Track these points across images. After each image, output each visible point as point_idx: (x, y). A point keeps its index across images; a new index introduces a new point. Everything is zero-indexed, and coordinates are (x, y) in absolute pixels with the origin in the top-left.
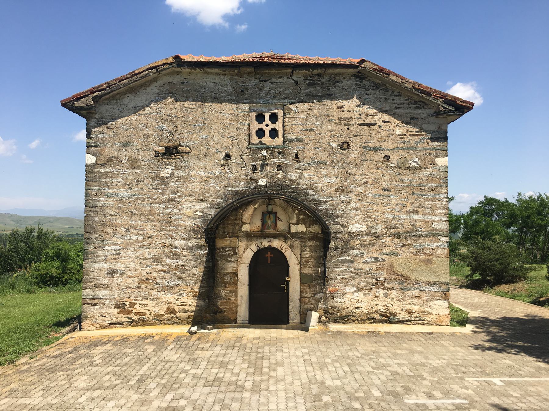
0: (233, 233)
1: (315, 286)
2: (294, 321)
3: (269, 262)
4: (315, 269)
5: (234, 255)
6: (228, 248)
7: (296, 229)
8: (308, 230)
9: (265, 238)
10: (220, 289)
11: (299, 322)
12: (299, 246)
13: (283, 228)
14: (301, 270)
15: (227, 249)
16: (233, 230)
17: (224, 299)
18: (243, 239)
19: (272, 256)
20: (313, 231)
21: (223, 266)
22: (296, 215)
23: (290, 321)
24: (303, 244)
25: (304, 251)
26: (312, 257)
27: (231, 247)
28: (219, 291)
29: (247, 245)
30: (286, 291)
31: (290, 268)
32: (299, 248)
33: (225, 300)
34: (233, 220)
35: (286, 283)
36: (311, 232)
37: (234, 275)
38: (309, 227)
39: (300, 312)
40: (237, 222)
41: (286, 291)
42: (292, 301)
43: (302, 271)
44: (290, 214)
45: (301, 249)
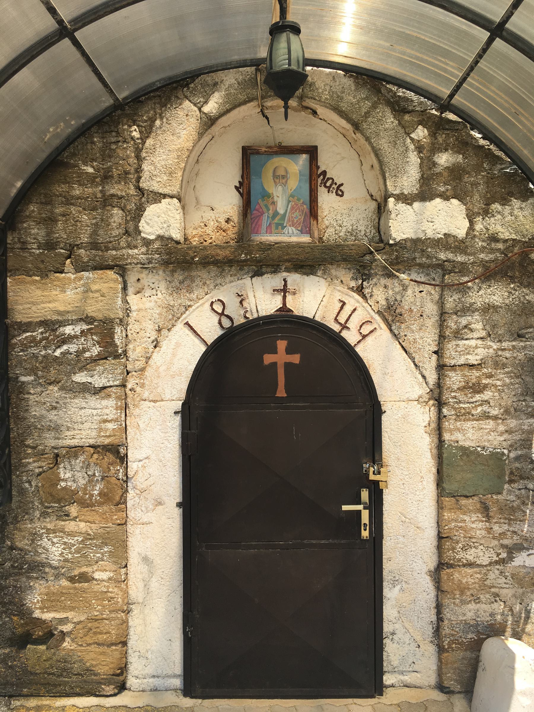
0: (94, 245)
1: (513, 510)
2: (407, 678)
3: (281, 392)
4: (513, 423)
5: (101, 358)
6: (73, 323)
7: (419, 222)
8: (479, 227)
9: (258, 273)
10: (38, 526)
11: (432, 679)
12: (431, 308)
13: (348, 224)
14: (439, 430)
15: (68, 330)
16: (95, 233)
17: (57, 577)
18: (147, 279)
19: (296, 359)
20: (505, 234)
21: (52, 416)
22: (419, 149)
23: (388, 679)
24: (451, 301)
25: (458, 335)
26: (497, 364)
27: (88, 320)
28: (35, 537)
29: (169, 308)
30: (365, 534)
31: (386, 421)
32: (431, 323)
33: (64, 583)
34: (92, 179)
35: (365, 495)
36: (494, 238)
37: (110, 457)
38: (486, 213)
39: (437, 631)
40: (115, 189)
41: (365, 534)
42: (394, 582)
43: (447, 436)
44: (384, 144)
45: (442, 324)
